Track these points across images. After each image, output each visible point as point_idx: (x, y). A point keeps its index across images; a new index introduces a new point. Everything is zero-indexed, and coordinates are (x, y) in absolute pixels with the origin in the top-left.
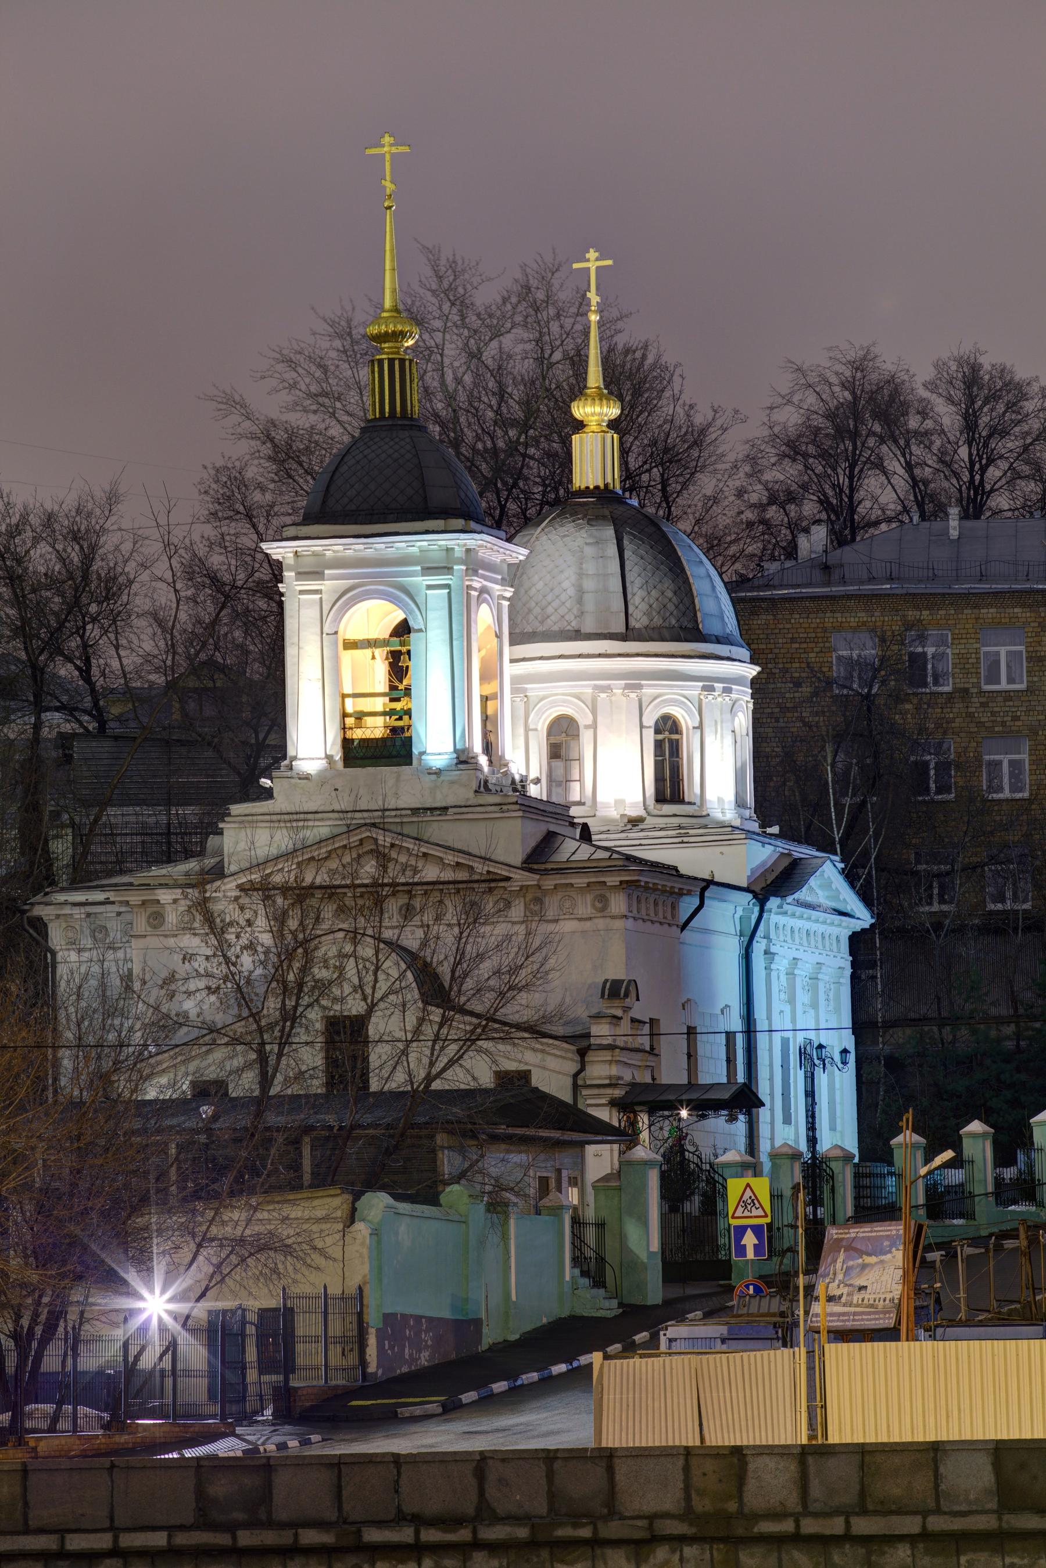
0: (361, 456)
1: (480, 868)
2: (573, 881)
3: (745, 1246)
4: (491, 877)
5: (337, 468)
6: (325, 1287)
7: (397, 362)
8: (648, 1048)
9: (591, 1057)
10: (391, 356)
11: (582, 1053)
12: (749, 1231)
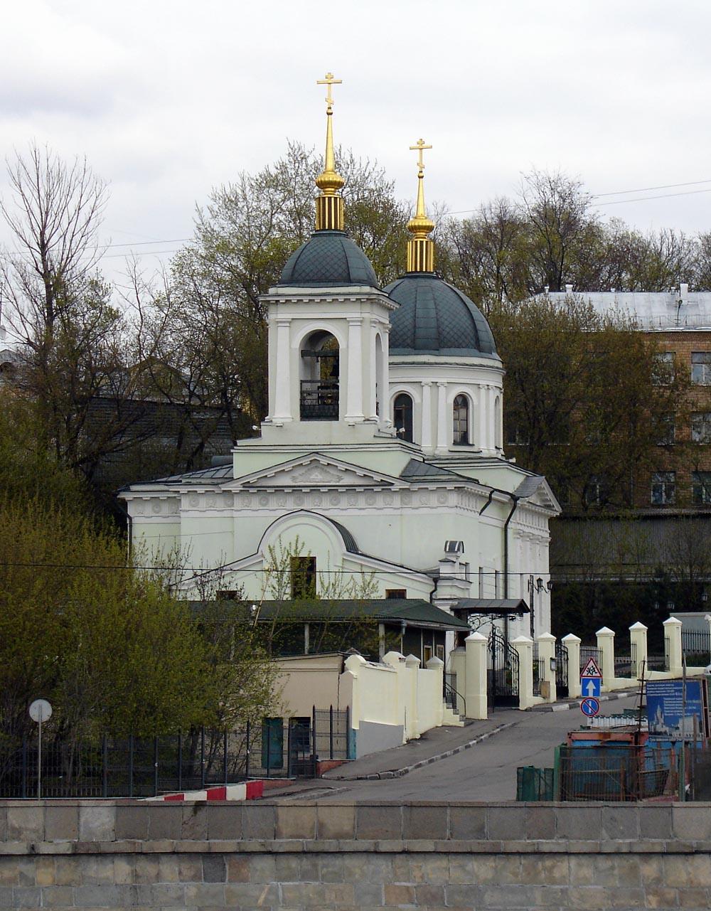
0: (458, 311)
1: (377, 478)
2: (357, 471)
3: (588, 690)
4: (383, 483)
5: (299, 257)
6: (331, 706)
7: (333, 199)
8: (464, 579)
9: (440, 583)
10: (329, 196)
11: (436, 580)
12: (591, 682)
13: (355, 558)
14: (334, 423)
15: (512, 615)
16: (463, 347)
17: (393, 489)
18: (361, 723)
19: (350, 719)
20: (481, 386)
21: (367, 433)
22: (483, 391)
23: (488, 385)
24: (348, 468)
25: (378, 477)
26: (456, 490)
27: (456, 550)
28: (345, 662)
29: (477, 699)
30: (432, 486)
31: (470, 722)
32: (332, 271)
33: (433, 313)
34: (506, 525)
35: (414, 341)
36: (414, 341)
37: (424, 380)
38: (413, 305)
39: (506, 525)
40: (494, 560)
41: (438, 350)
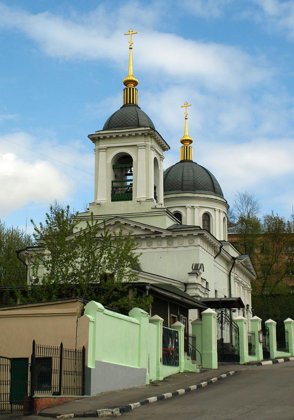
1: (153, 230)
6: (62, 344)
13: (183, 336)
14: (129, 202)
15: (233, 309)
16: (206, 190)
17: (163, 236)
18: (98, 363)
19: (86, 355)
20: (216, 210)
21: (148, 207)
22: (217, 212)
23: (220, 210)
24: (136, 225)
25: (153, 229)
26: (199, 236)
27: (199, 268)
28: (85, 307)
29: (211, 355)
30: (185, 234)
31: (203, 371)
32: (129, 121)
33: (192, 174)
34: (230, 273)
35: (182, 187)
36: (182, 187)
37: (187, 205)
38: (182, 171)
39: (230, 273)
40: (224, 289)
41: (194, 191)
